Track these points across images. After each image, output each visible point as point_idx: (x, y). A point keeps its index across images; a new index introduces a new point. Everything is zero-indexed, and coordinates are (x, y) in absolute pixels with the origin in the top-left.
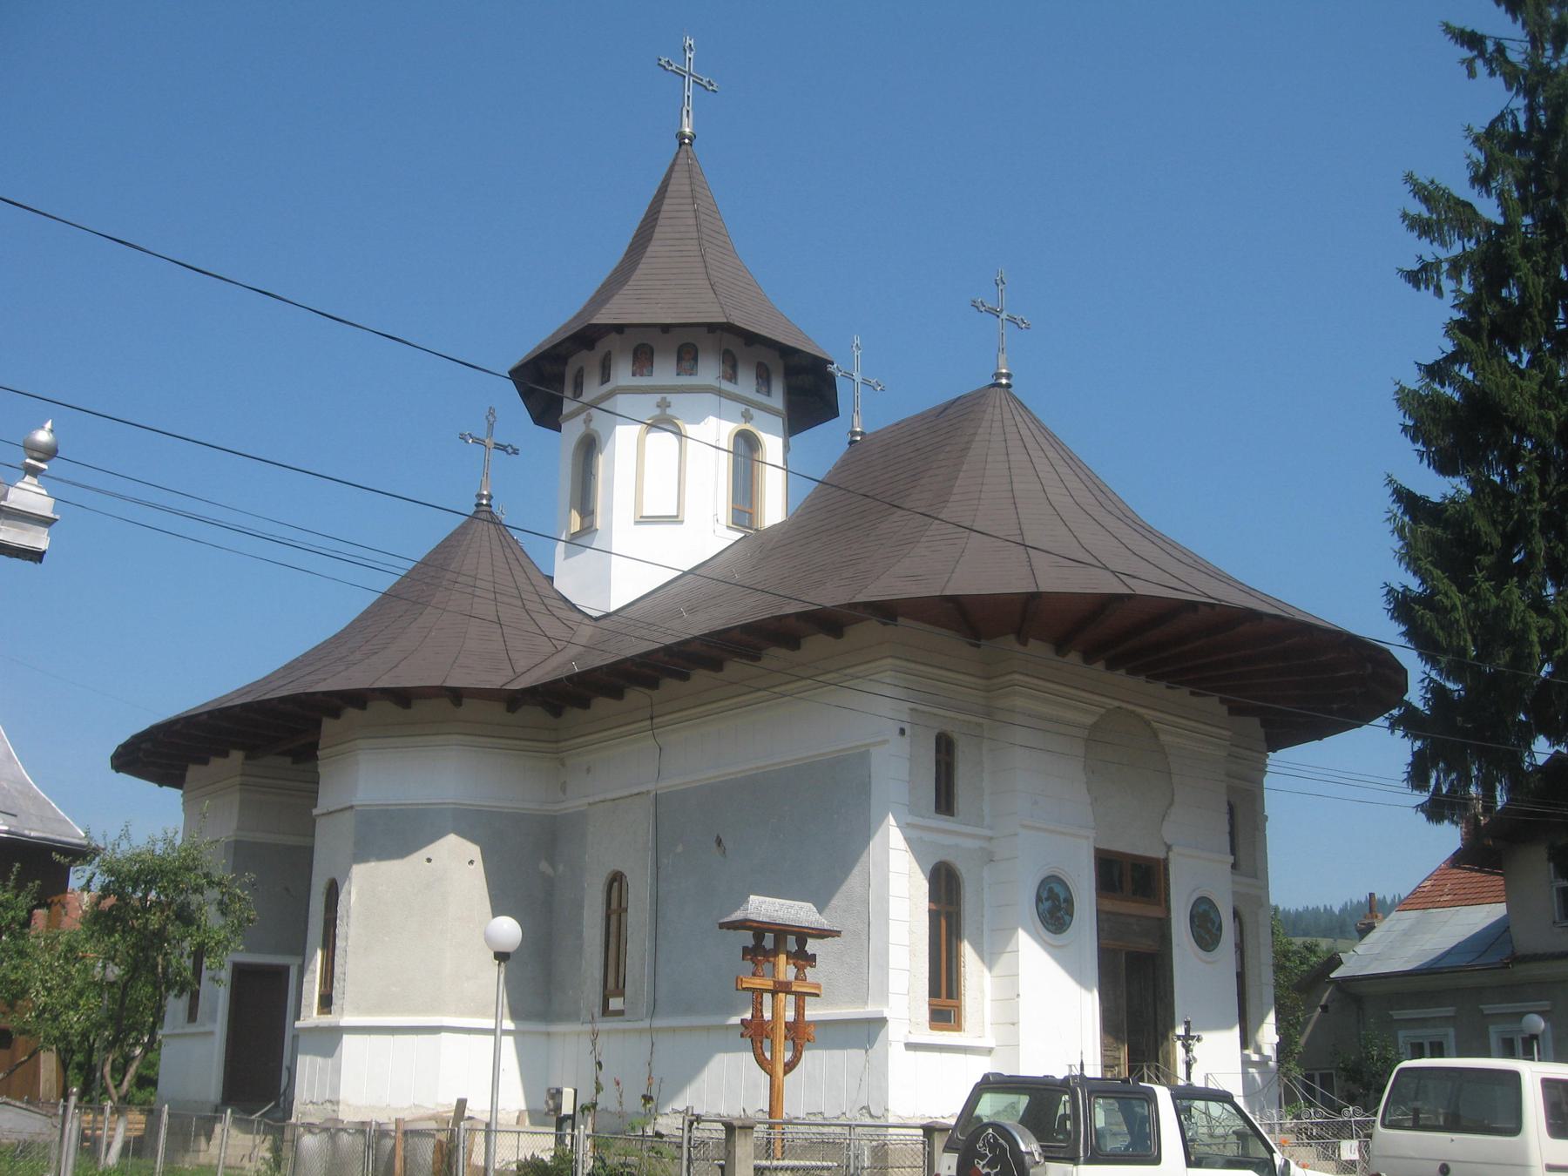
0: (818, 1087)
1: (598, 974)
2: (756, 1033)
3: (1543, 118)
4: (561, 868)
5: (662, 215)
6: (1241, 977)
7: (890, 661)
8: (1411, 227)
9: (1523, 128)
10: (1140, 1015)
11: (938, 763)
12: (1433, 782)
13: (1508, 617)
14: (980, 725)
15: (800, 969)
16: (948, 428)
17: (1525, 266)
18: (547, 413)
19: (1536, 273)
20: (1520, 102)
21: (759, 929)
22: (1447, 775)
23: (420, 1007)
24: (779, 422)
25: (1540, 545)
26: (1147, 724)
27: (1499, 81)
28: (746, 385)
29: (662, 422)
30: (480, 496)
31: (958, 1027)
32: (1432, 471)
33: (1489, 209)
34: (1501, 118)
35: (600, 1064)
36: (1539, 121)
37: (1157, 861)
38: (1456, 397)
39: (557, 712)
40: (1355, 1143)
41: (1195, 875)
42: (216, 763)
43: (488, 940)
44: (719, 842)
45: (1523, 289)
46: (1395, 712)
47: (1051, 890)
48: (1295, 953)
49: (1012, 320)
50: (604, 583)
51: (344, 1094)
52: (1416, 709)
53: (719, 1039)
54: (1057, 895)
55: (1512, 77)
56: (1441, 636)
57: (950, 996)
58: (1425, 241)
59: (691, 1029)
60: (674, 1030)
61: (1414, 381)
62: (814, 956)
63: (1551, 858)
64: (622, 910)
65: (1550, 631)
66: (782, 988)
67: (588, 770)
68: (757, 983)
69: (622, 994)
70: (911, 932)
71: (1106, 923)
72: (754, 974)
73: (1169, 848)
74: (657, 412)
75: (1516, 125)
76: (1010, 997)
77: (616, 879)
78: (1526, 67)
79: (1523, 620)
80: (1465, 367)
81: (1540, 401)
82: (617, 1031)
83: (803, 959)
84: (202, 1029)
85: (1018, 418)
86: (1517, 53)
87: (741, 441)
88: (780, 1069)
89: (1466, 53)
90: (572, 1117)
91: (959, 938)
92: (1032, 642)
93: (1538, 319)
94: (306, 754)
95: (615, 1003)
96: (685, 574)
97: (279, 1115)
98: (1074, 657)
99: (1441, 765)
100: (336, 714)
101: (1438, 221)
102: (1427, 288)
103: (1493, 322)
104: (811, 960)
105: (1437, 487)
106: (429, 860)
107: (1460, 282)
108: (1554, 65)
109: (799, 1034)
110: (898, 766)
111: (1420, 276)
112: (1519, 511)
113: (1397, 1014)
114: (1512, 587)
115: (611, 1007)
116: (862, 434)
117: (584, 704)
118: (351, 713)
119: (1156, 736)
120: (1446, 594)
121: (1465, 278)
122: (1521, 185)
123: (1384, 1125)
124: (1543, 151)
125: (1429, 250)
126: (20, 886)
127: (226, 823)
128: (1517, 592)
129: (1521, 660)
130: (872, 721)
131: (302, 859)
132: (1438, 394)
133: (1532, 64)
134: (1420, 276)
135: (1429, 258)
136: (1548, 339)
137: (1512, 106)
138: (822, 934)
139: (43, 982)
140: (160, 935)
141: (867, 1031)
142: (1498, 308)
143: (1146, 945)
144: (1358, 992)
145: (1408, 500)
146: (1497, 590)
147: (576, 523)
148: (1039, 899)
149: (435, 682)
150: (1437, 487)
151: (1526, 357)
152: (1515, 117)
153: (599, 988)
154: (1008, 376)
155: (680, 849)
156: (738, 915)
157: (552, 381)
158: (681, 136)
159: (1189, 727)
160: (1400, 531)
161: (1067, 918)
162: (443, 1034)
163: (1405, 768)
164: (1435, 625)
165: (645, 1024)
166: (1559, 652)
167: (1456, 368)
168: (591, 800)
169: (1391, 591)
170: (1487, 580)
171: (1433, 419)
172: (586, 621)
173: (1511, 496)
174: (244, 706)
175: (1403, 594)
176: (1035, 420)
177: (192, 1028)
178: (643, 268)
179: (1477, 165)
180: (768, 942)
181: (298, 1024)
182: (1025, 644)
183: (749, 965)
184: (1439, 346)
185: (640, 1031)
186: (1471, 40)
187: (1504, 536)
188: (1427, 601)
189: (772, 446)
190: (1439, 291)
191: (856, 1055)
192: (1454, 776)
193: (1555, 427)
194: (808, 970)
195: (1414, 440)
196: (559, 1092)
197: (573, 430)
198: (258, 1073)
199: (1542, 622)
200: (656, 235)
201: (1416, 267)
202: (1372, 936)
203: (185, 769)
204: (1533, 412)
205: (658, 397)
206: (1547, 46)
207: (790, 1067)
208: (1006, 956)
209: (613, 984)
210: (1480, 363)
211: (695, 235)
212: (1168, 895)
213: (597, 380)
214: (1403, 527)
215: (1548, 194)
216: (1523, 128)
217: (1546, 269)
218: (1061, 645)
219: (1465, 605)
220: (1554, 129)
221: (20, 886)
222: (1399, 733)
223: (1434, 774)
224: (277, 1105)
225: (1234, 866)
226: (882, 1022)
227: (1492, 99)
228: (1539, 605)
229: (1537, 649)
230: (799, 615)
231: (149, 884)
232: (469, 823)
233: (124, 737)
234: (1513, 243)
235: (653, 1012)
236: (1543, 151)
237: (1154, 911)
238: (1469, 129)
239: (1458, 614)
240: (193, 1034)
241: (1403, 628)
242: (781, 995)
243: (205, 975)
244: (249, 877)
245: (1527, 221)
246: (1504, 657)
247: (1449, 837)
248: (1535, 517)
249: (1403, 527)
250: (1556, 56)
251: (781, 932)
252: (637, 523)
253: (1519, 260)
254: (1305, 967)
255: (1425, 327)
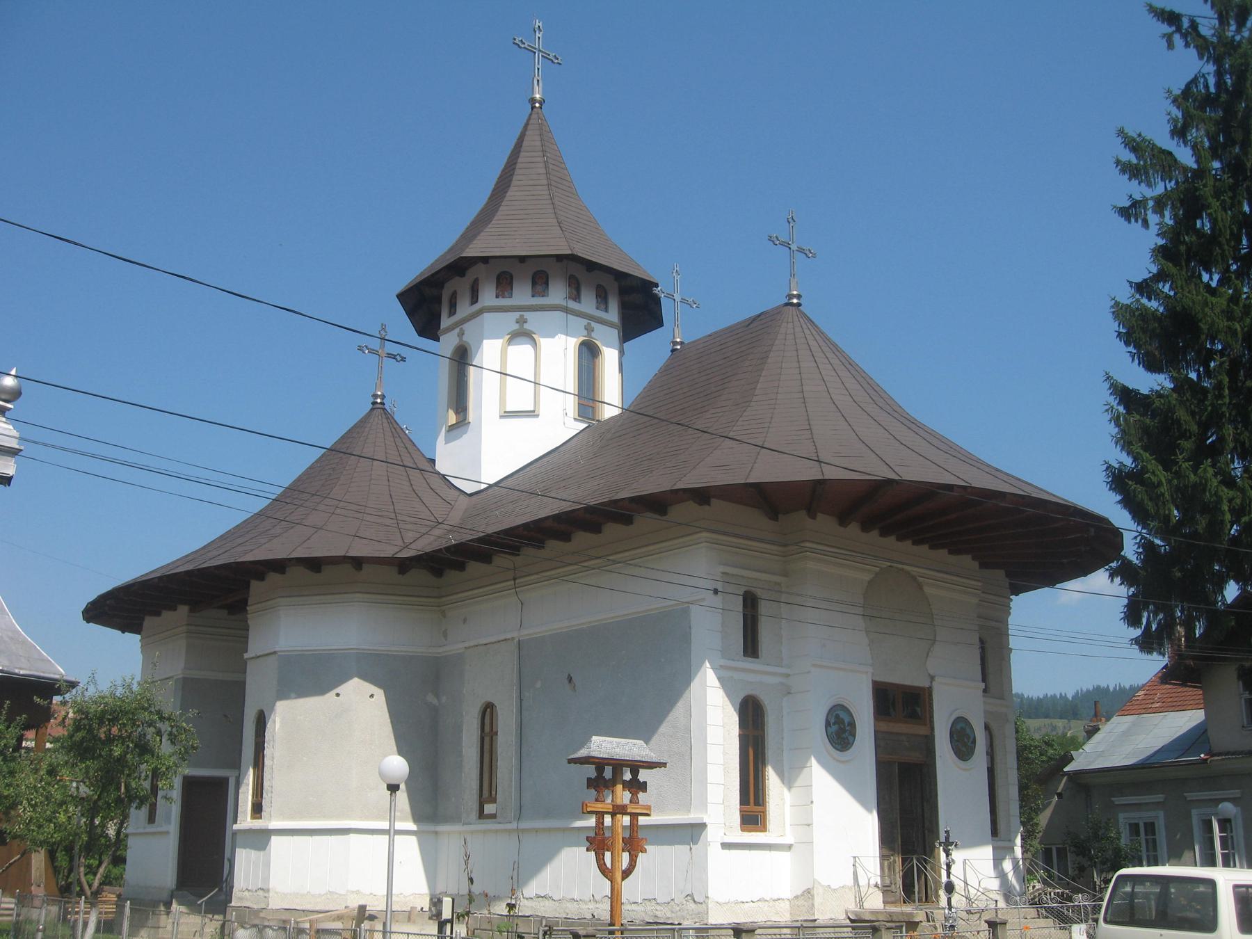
0: (653, 882)
1: (475, 785)
2: (598, 843)
3: (1229, 81)
4: (444, 699)
5: (518, 166)
6: (991, 772)
7: (705, 534)
8: (1123, 171)
9: (1212, 90)
10: (911, 833)
11: (745, 617)
12: (1144, 621)
13: (1204, 490)
14: (779, 584)
15: (634, 795)
16: (749, 342)
17: (1216, 204)
18: (428, 326)
19: (1224, 209)
20: (1210, 68)
21: (600, 764)
22: (1156, 615)
23: (333, 814)
24: (614, 334)
25: (1229, 430)
26: (914, 578)
27: (1192, 52)
28: (588, 303)
29: (522, 334)
30: (375, 396)
31: (764, 828)
32: (1141, 369)
33: (1185, 156)
34: (1194, 81)
35: (471, 880)
36: (1225, 83)
37: (922, 689)
38: (1161, 309)
39: (438, 573)
40: (1083, 926)
41: (955, 698)
42: (166, 614)
43: (382, 775)
44: (570, 680)
45: (1214, 222)
46: (1114, 565)
47: (837, 716)
48: (1036, 747)
49: (801, 250)
50: (476, 462)
51: (273, 884)
52: (1130, 562)
53: (569, 836)
54: (842, 722)
55: (1203, 46)
56: (1150, 506)
57: (757, 803)
58: (1135, 182)
59: (549, 830)
60: (537, 830)
61: (1126, 296)
62: (645, 783)
63: (1240, 677)
64: (493, 734)
65: (1238, 501)
66: (618, 810)
67: (465, 621)
68: (599, 807)
69: (494, 801)
70: (725, 753)
71: (882, 742)
72: (597, 800)
73: (932, 678)
74: (516, 327)
75: (1206, 87)
76: (807, 803)
77: (488, 711)
78: (1215, 39)
79: (1216, 494)
80: (1167, 286)
81: (1229, 316)
82: (490, 831)
83: (637, 786)
84: (159, 829)
85: (807, 332)
86: (1208, 28)
87: (585, 349)
88: (618, 875)
89: (1167, 29)
90: (451, 921)
91: (764, 764)
92: (820, 516)
93: (1226, 247)
94: (239, 607)
95: (489, 808)
96: (490, 486)
97: (223, 897)
98: (853, 529)
99: (1151, 607)
100: (261, 577)
101: (1145, 166)
102: (1136, 221)
103: (1189, 250)
104: (643, 787)
105: (1147, 382)
106: (338, 695)
107: (1163, 216)
108: (1238, 38)
109: (633, 845)
110: (712, 623)
111: (1132, 211)
112: (1212, 405)
113: (1118, 800)
114: (1207, 469)
115: (486, 812)
116: (681, 343)
117: (461, 567)
118: (273, 577)
119: (920, 587)
120: (1153, 473)
121: (1167, 213)
122: (1212, 138)
123: (1106, 921)
124: (1229, 110)
125: (1138, 190)
126: (10, 720)
127: (175, 665)
128: (1211, 471)
129: (1216, 527)
130: (691, 580)
131: (234, 693)
132: (1146, 309)
133: (1219, 37)
134: (1132, 211)
135: (1138, 197)
136: (1236, 260)
137: (1204, 71)
138: (651, 765)
139: (29, 800)
140: (121, 760)
141: (692, 832)
142: (1194, 238)
143: (915, 757)
144: (1086, 783)
145: (1126, 395)
146: (1195, 469)
147: (452, 418)
148: (828, 724)
149: (342, 553)
150: (1147, 382)
151: (1216, 277)
152: (1206, 80)
153: (476, 797)
154: (799, 297)
155: (539, 685)
156: (583, 753)
157: (430, 302)
158: (533, 101)
159: (948, 583)
160: (1116, 420)
161: (850, 738)
162: (352, 836)
163: (1122, 609)
164: (1145, 497)
165: (514, 825)
166: (1245, 519)
167: (1161, 285)
168: (467, 644)
169: (1109, 467)
170: (1188, 460)
171: (1142, 328)
172: (462, 497)
173: (1205, 391)
174: (188, 573)
175: (1120, 470)
176: (821, 333)
177: (151, 829)
178: (503, 210)
179: (1175, 120)
180: (606, 775)
181: (235, 827)
182: (813, 517)
183: (593, 792)
184: (1145, 267)
185: (509, 831)
186: (1171, 18)
187: (1199, 424)
188: (1137, 476)
189: (610, 357)
190: (1146, 224)
191: (682, 849)
192: (1161, 616)
193: (1240, 336)
194: (641, 795)
195: (1127, 344)
196: (440, 901)
197: (448, 343)
198: (204, 868)
199: (1231, 493)
200: (514, 183)
201: (1128, 204)
202: (1097, 737)
203: (143, 619)
204: (1223, 323)
205: (517, 315)
206: (1232, 22)
207: (626, 874)
208: (806, 770)
209: (487, 793)
210: (1179, 283)
211: (545, 182)
212: (932, 717)
213: (467, 301)
214: (1118, 417)
215: (1234, 143)
216: (1212, 90)
217: (1233, 205)
218: (843, 518)
219: (1169, 482)
220: (1238, 92)
221: (10, 720)
222: (1117, 580)
223: (1145, 614)
224: (221, 890)
225: (985, 691)
226: (703, 826)
227: (1187, 65)
228: (1229, 482)
229: (1228, 517)
230: (632, 499)
231: (114, 720)
232: (375, 668)
233: (92, 597)
234: (1205, 186)
235: (519, 817)
236: (1229, 110)
237: (923, 731)
238: (1169, 91)
239: (1164, 489)
240: (154, 834)
241: (1119, 498)
242: (619, 816)
243: (160, 794)
244: (193, 712)
245: (1216, 165)
246: (1202, 523)
247: (1156, 663)
248: (1224, 409)
249: (1118, 417)
250: (1239, 31)
251: (618, 765)
252: (501, 417)
253: (1210, 200)
254: (1044, 758)
255: (1135, 252)
